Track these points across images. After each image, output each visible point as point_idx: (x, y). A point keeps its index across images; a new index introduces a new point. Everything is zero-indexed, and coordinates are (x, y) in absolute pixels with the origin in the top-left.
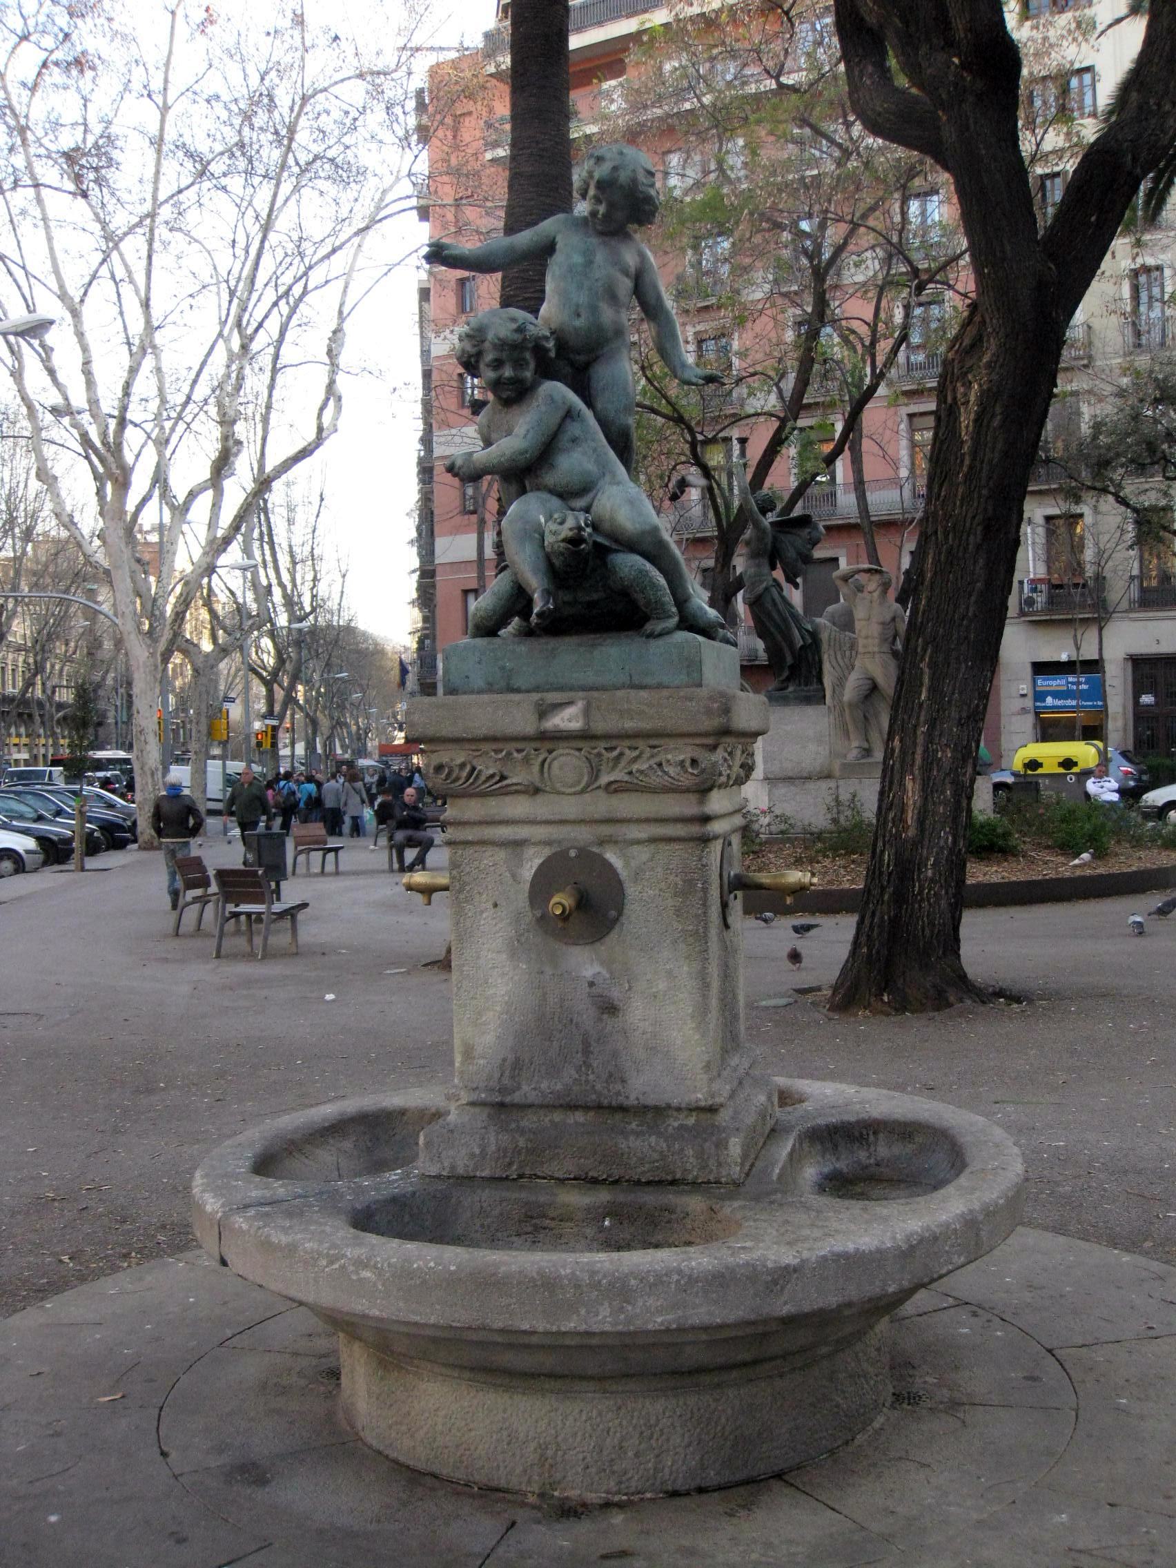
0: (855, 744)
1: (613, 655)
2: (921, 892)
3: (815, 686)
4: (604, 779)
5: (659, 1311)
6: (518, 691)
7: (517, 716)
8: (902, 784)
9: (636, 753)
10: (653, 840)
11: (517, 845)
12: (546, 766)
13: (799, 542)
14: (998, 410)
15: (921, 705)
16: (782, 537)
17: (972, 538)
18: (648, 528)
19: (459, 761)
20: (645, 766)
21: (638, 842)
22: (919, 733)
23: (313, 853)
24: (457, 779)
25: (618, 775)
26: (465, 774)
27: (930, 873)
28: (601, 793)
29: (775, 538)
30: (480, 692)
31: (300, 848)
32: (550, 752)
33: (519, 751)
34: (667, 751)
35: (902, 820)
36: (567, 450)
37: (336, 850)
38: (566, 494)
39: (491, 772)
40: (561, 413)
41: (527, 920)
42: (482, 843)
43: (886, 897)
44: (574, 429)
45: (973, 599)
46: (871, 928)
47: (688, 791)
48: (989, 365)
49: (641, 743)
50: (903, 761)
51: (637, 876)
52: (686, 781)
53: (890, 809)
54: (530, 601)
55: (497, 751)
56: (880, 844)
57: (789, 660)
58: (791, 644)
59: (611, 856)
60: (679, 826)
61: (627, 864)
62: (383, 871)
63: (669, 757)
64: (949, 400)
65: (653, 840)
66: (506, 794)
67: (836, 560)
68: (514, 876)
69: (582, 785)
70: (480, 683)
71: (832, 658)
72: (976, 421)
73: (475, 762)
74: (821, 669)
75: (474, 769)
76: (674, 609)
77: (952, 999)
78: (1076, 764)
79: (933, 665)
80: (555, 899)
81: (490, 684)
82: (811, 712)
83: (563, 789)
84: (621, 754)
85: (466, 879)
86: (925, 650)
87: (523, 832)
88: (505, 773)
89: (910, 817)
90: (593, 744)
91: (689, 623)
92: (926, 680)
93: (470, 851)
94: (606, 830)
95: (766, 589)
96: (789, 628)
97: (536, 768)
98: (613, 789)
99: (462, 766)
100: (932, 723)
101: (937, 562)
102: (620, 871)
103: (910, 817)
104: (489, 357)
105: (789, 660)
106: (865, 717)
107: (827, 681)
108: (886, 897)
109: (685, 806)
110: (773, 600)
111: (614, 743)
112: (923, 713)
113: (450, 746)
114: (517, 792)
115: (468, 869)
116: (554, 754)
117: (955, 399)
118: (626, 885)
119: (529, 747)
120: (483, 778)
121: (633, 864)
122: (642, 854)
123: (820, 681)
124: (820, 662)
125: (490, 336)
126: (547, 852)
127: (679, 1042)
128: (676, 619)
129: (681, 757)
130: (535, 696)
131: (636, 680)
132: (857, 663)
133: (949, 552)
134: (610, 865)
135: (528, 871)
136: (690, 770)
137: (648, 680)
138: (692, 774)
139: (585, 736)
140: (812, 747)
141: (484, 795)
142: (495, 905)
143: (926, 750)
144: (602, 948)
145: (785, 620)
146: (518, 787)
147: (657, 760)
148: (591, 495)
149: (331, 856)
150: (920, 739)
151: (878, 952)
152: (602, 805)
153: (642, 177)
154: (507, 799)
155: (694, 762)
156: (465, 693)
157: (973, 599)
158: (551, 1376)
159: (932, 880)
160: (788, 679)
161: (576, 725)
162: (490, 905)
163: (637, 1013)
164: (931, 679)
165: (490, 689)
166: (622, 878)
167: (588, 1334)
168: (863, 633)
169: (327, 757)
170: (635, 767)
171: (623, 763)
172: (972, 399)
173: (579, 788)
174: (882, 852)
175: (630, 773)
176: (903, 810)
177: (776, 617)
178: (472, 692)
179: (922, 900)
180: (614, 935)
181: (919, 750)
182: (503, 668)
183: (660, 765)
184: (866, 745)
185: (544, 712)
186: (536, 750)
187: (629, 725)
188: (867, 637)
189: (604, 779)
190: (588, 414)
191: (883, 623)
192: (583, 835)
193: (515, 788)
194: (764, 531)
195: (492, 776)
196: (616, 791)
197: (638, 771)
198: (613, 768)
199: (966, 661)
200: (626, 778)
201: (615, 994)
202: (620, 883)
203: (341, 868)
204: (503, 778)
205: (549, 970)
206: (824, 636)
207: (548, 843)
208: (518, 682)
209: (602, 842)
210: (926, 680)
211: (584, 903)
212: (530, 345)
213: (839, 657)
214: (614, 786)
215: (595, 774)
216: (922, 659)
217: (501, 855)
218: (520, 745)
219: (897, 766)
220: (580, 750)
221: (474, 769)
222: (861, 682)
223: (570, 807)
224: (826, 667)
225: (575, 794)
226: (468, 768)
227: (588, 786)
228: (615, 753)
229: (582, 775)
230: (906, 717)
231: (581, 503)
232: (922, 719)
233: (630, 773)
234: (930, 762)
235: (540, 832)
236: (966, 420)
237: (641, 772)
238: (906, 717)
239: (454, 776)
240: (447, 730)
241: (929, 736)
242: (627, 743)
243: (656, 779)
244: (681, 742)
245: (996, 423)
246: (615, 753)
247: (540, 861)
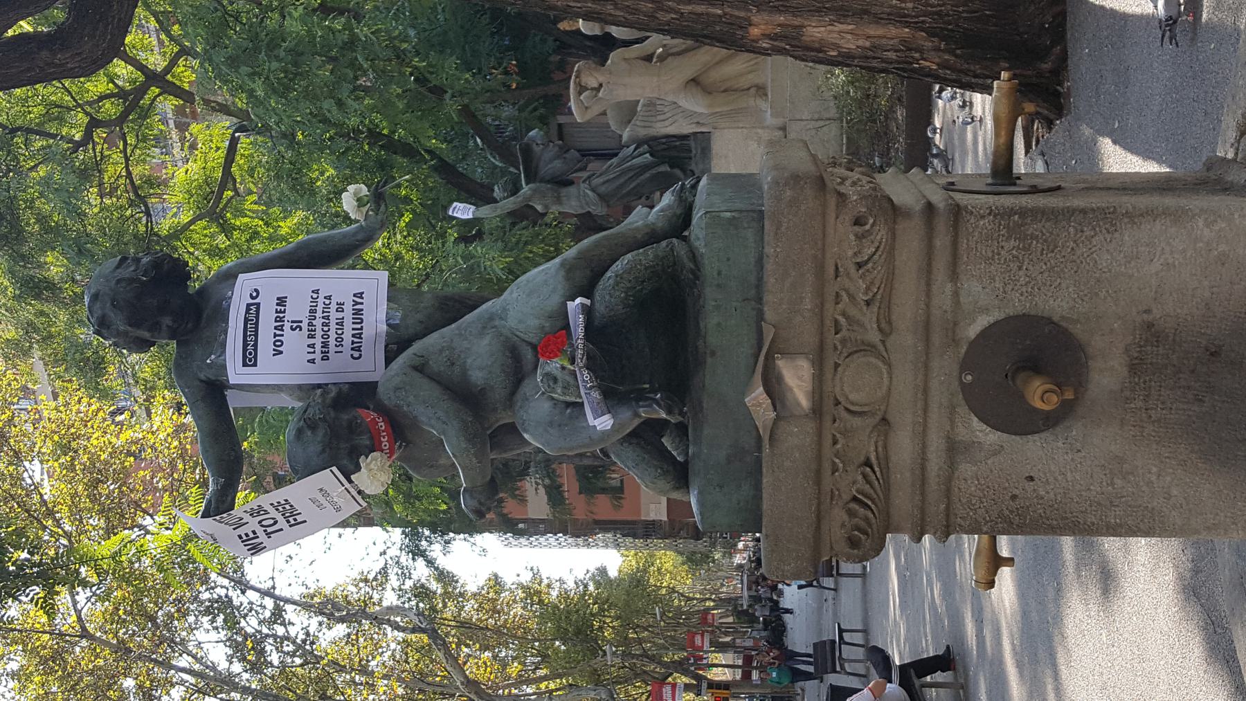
1: (720, 324)
3: (693, 144)
4: (874, 337)
9: (843, 294)
10: (954, 276)
11: (954, 449)
13: (548, 155)
18: (562, 273)
19: (845, 517)
23: (844, 656)
24: (867, 519)
25: (869, 318)
29: (541, 181)
30: (758, 487)
31: (838, 669)
32: (838, 403)
33: (835, 442)
36: (464, 372)
37: (841, 631)
38: (517, 373)
39: (860, 477)
40: (416, 375)
42: (948, 493)
44: (436, 365)
47: (893, 235)
49: (831, 289)
52: (881, 233)
54: (648, 423)
56: (874, 64)
57: (665, 168)
58: (646, 167)
59: (973, 331)
60: (938, 243)
61: (985, 310)
62: (864, 583)
63: (850, 253)
65: (954, 276)
66: (887, 458)
67: (560, 125)
68: (995, 453)
69: (880, 364)
71: (667, 123)
73: (846, 497)
74: (674, 136)
75: (855, 499)
76: (664, 243)
80: (1038, 404)
83: (885, 388)
84: (844, 314)
87: (936, 444)
88: (862, 459)
91: (681, 222)
95: (593, 190)
96: (630, 169)
97: (857, 421)
98: (886, 328)
102: (992, 320)
105: (665, 168)
107: (687, 129)
109: (910, 239)
110: (604, 183)
111: (829, 323)
114: (885, 447)
116: (841, 399)
119: (829, 429)
124: (667, 136)
126: (963, 410)
128: (675, 240)
129: (852, 237)
132: (670, 98)
134: (984, 334)
135: (991, 437)
136: (867, 227)
137: (752, 279)
138: (873, 225)
139: (819, 363)
141: (887, 489)
142: (1031, 479)
145: (623, 173)
146: (880, 443)
147: (853, 270)
149: (847, 637)
152: (905, 339)
153: (127, 272)
154: (894, 458)
155: (858, 222)
160: (684, 171)
166: (1003, 316)
169: (736, 632)
171: (853, 312)
173: (884, 369)
174: (883, 61)
175: (868, 303)
177: (622, 180)
180: (1077, 330)
183: (859, 265)
184: (753, 91)
186: (834, 421)
189: (874, 337)
190: (417, 347)
192: (945, 367)
193: (880, 449)
194: (535, 191)
195: (865, 476)
196: (890, 323)
197: (866, 293)
198: (862, 325)
202: (1008, 319)
203: (860, 627)
204: (867, 463)
206: (642, 132)
207: (952, 409)
209: (955, 342)
211: (1032, 365)
212: (332, 414)
213: (662, 117)
214: (883, 325)
215: (866, 348)
218: (828, 441)
220: (837, 366)
221: (855, 499)
223: (905, 381)
224: (672, 130)
226: (854, 506)
227: (880, 356)
228: (842, 320)
231: (528, 354)
235: (936, 417)
239: (863, 524)
242: (829, 306)
246: (842, 320)
247: (976, 419)
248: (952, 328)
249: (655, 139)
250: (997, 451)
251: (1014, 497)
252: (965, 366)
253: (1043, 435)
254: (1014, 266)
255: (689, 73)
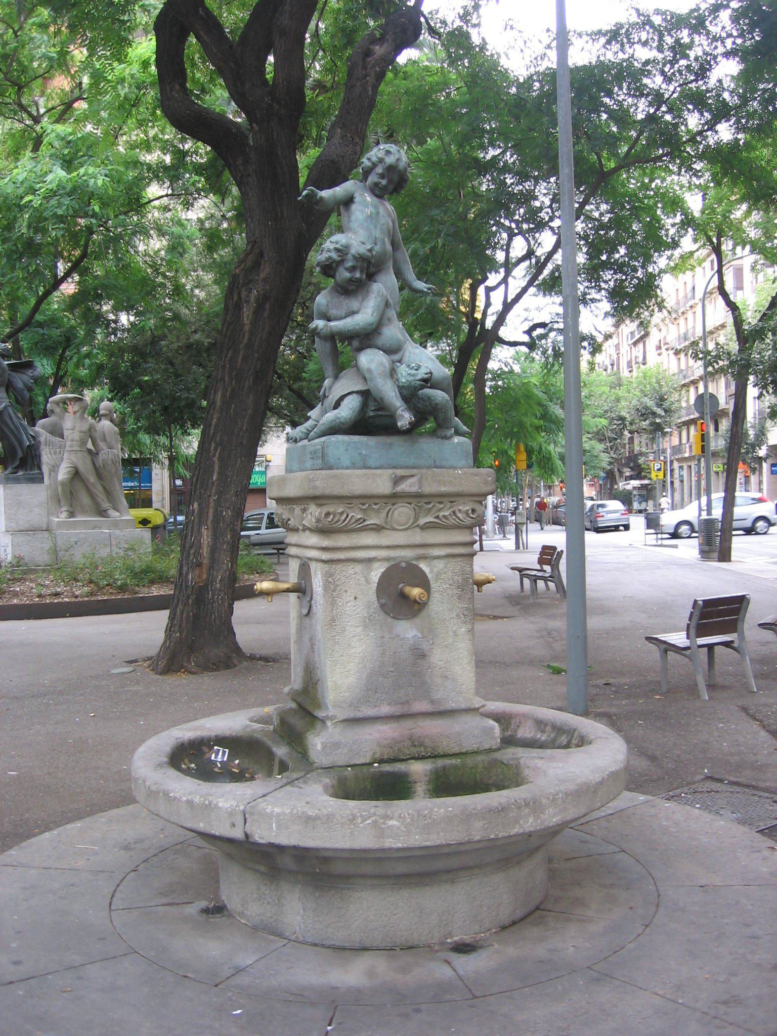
0: (65, 509)
2: (213, 598)
5: (554, 815)
6: (370, 468)
7: (381, 483)
8: (199, 531)
11: (370, 560)
12: (390, 514)
14: (267, 306)
15: (213, 483)
16: (14, 374)
17: (247, 383)
20: (447, 513)
21: (438, 557)
22: (211, 500)
24: (338, 521)
26: (343, 518)
27: (218, 586)
28: (418, 530)
30: (347, 468)
32: (393, 504)
33: (376, 504)
34: (459, 505)
35: (201, 555)
41: (374, 606)
43: (190, 601)
45: (246, 420)
46: (181, 621)
48: (264, 280)
50: (200, 517)
51: (437, 576)
53: (191, 547)
55: (363, 504)
56: (185, 569)
57: (20, 454)
58: (20, 442)
59: (423, 566)
64: (235, 298)
68: (367, 580)
70: (346, 463)
72: (254, 312)
77: (235, 661)
78: (150, 522)
79: (221, 459)
81: (354, 464)
82: (35, 487)
85: (337, 583)
86: (216, 450)
89: (205, 551)
90: (418, 500)
92: (216, 467)
93: (339, 567)
94: (420, 551)
97: (384, 514)
98: (424, 528)
99: (342, 513)
100: (220, 494)
101: (224, 396)
103: (205, 551)
104: (349, 264)
106: (71, 492)
107: (45, 469)
108: (190, 601)
112: (214, 488)
113: (335, 501)
115: (339, 577)
117: (240, 297)
118: (431, 582)
120: (353, 520)
121: (435, 570)
122: (440, 565)
123: (40, 468)
125: (353, 251)
127: (459, 672)
130: (390, 471)
131: (438, 463)
133: (233, 390)
134: (423, 572)
140: (37, 511)
142: (356, 598)
143: (216, 510)
144: (417, 620)
147: (452, 509)
148: (401, 353)
150: (212, 504)
151: (186, 636)
152: (418, 537)
155: (473, 511)
156: (337, 469)
157: (246, 420)
158: (372, 877)
159: (220, 590)
161: (414, 489)
162: (352, 598)
163: (437, 657)
164: (220, 467)
165: (354, 466)
167: (510, 836)
168: (70, 438)
170: (441, 514)
172: (252, 299)
174: (187, 574)
176: (200, 547)
177: (12, 426)
178: (343, 468)
179: (214, 602)
181: (211, 511)
182: (360, 454)
183: (454, 512)
185: (397, 480)
187: (443, 489)
188: (72, 441)
189: (422, 521)
191: (81, 432)
192: (408, 554)
199: (241, 457)
200: (435, 520)
201: (425, 646)
204: (364, 520)
205: (387, 636)
206: (42, 439)
208: (371, 462)
210: (216, 467)
215: (416, 519)
216: (214, 455)
217: (358, 568)
218: (376, 501)
219: (197, 520)
220: (410, 504)
222: (69, 469)
225: (407, 529)
227: (413, 524)
229: (409, 519)
230: (203, 491)
232: (213, 491)
233: (437, 517)
234: (217, 517)
236: (247, 313)
237: (444, 516)
238: (203, 491)
240: (337, 491)
241: (218, 503)
242: (438, 499)
243: (452, 521)
244: (466, 499)
245: (266, 314)
246: (430, 506)
247: (383, 570)
248: (424, 558)
249: (39, 447)
250: (367, 581)
251: (346, 591)
252: (408, 563)
253: (376, 602)
254: (451, 582)
255: (81, 468)
